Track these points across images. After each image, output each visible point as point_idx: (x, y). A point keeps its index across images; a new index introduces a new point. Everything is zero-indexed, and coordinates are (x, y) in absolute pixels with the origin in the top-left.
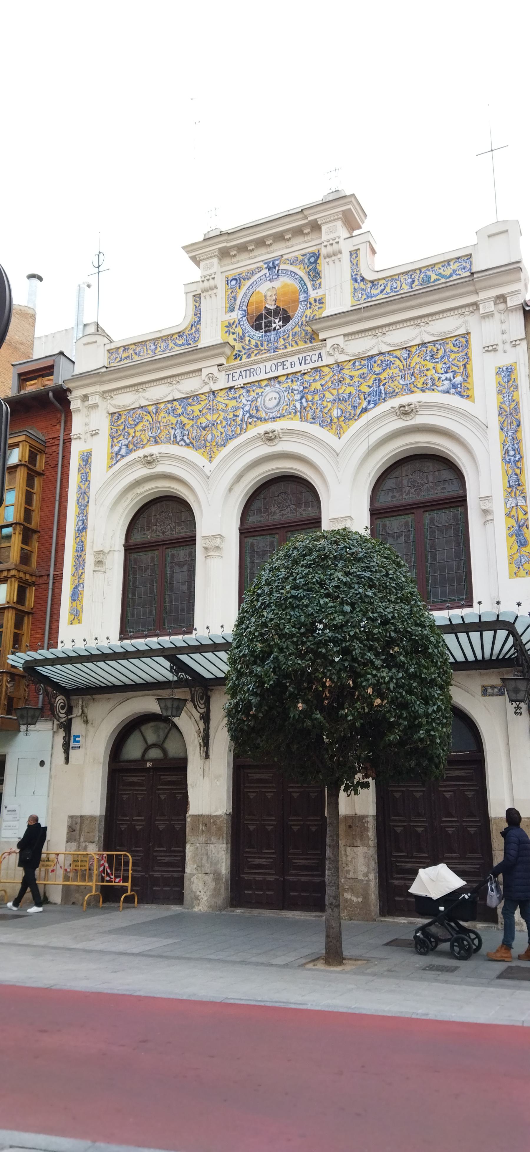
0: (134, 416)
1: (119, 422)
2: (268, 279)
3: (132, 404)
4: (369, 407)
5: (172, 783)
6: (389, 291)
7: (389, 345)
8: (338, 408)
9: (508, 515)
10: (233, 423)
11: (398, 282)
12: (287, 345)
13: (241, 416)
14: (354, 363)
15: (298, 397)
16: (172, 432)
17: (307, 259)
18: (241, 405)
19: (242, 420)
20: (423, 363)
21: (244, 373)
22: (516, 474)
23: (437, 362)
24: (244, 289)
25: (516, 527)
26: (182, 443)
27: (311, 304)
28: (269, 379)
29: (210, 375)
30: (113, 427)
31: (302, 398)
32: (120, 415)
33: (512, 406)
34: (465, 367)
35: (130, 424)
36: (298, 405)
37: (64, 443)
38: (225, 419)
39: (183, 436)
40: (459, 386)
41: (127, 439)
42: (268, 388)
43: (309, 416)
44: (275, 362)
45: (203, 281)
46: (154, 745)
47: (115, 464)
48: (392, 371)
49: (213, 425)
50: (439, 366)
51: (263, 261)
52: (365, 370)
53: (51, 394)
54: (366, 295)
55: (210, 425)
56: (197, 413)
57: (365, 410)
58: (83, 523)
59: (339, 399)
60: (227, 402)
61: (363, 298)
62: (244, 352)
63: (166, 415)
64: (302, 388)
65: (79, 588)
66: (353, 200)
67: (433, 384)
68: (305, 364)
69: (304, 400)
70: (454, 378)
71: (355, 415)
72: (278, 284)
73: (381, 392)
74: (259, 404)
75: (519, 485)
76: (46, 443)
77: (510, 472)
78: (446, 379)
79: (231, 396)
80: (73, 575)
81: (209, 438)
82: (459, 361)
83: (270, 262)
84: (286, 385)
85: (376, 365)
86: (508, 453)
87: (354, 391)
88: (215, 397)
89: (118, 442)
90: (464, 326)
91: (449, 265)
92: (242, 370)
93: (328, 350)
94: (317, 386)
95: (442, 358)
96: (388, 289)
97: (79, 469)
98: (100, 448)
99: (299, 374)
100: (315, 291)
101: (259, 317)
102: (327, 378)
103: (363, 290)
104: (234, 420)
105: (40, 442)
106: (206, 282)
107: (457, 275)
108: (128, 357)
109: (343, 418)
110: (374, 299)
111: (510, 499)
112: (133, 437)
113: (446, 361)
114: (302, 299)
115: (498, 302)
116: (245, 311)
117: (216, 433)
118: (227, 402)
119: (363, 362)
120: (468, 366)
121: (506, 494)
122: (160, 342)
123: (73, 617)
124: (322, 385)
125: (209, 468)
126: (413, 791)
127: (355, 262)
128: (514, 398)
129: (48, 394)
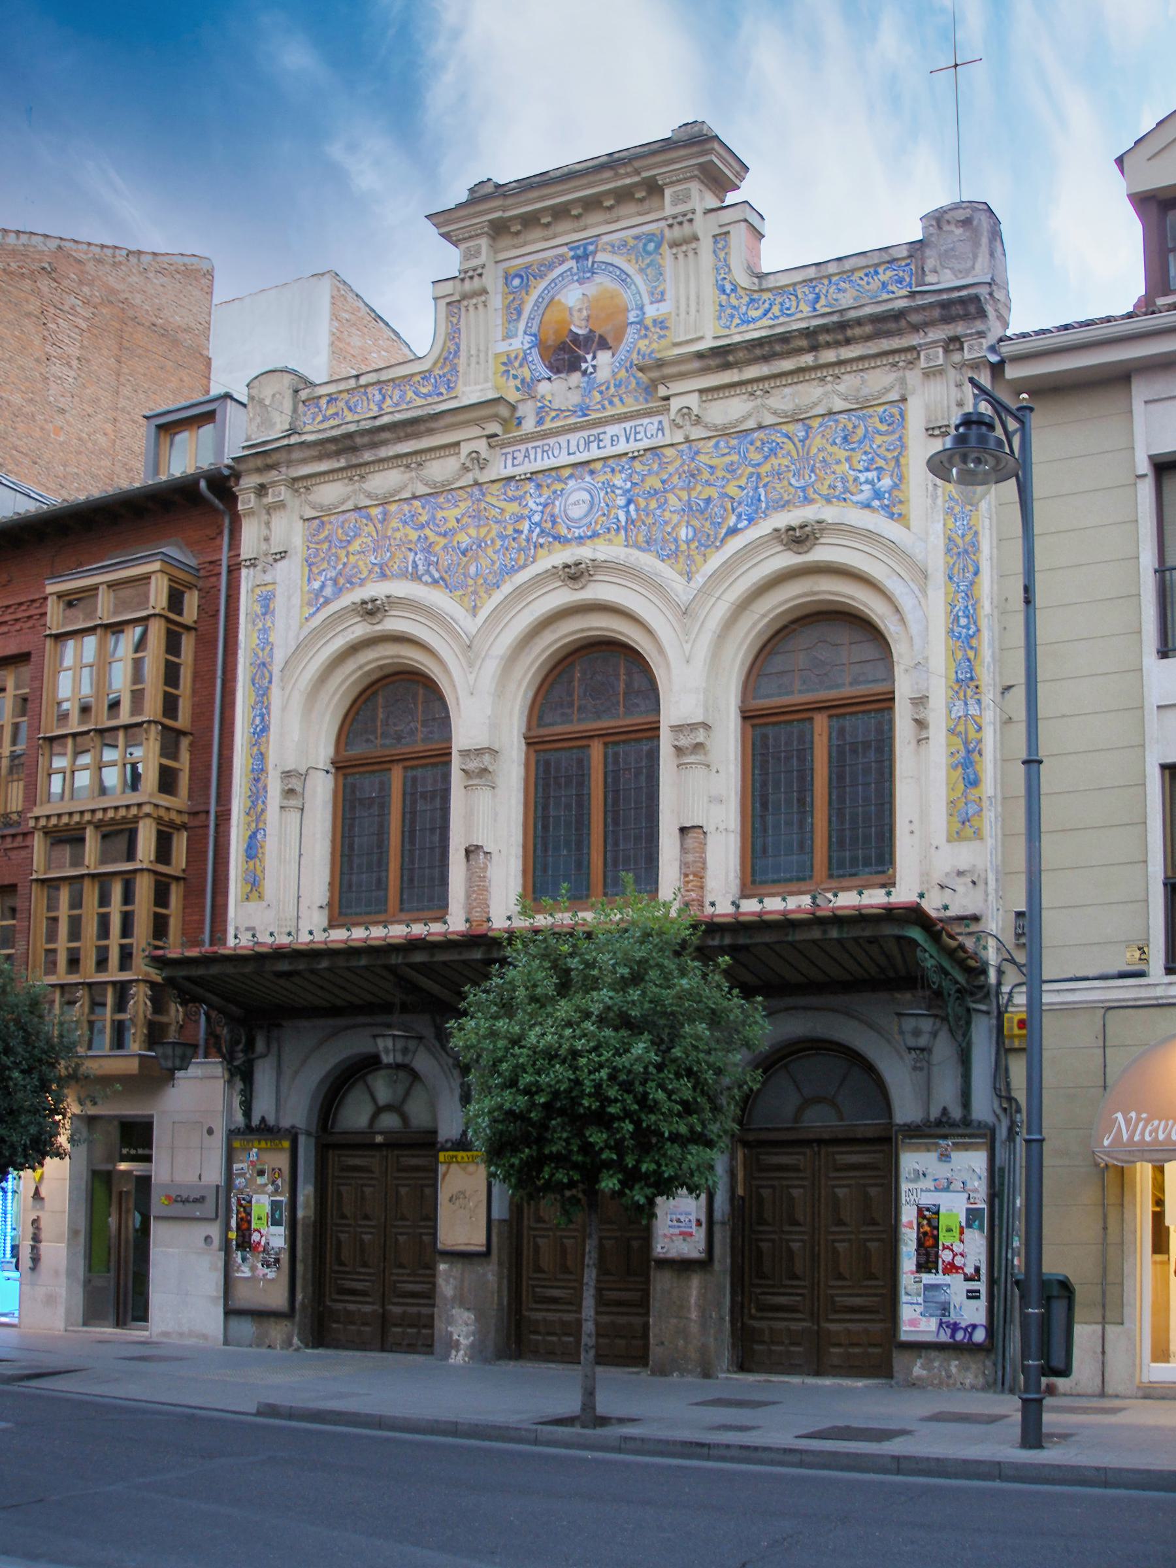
3: (342, 503)
5: (417, 1169)
6: (778, 314)
7: (775, 413)
8: (688, 524)
9: (952, 731)
10: (514, 545)
11: (793, 298)
12: (606, 402)
13: (526, 532)
14: (718, 443)
15: (621, 501)
16: (411, 556)
17: (641, 245)
18: (526, 512)
19: (528, 540)
20: (830, 449)
21: (532, 453)
22: (969, 660)
23: (853, 450)
24: (535, 294)
25: (963, 753)
26: (426, 578)
27: (647, 328)
28: (574, 465)
29: (474, 455)
30: (311, 545)
31: (629, 502)
32: (323, 523)
33: (968, 538)
35: (341, 541)
36: (622, 518)
37: (230, 572)
38: (502, 537)
39: (429, 565)
40: (887, 495)
41: (335, 568)
42: (572, 483)
43: (641, 539)
44: (585, 434)
45: (463, 280)
46: (389, 1108)
47: (314, 613)
48: (780, 461)
49: (480, 546)
51: (567, 244)
52: (735, 458)
53: (203, 484)
54: (740, 318)
55: (474, 547)
56: (452, 523)
57: (733, 531)
58: (262, 720)
59: (691, 508)
60: (503, 504)
61: (734, 324)
63: (400, 525)
65: (259, 837)
66: (716, 146)
67: (846, 490)
68: (636, 440)
69: (632, 507)
70: (879, 480)
71: (716, 538)
72: (591, 289)
73: (759, 500)
74: (557, 511)
75: (972, 679)
76: (198, 570)
77: (959, 655)
78: (867, 482)
79: (510, 494)
80: (248, 814)
81: (472, 570)
82: (888, 450)
83: (578, 248)
84: (602, 479)
85: (752, 448)
86: (958, 621)
87: (716, 495)
88: (484, 495)
89: (320, 573)
90: (897, 388)
91: (877, 273)
92: (530, 445)
93: (672, 417)
94: (654, 482)
95: (860, 442)
96: (776, 310)
98: (288, 577)
99: (624, 459)
100: (656, 306)
101: (562, 347)
102: (671, 469)
103: (734, 307)
104: (514, 539)
105: (187, 569)
106: (467, 281)
107: (888, 292)
108: (337, 414)
110: (752, 326)
111: (958, 703)
112: (345, 564)
113: (868, 449)
114: (632, 319)
115: (951, 347)
116: (535, 335)
117: (485, 562)
118: (503, 504)
119: (733, 442)
120: (902, 460)
121: (951, 693)
122: (390, 388)
124: (663, 482)
125: (469, 624)
126: (788, 1187)
128: (972, 523)
129: (197, 483)
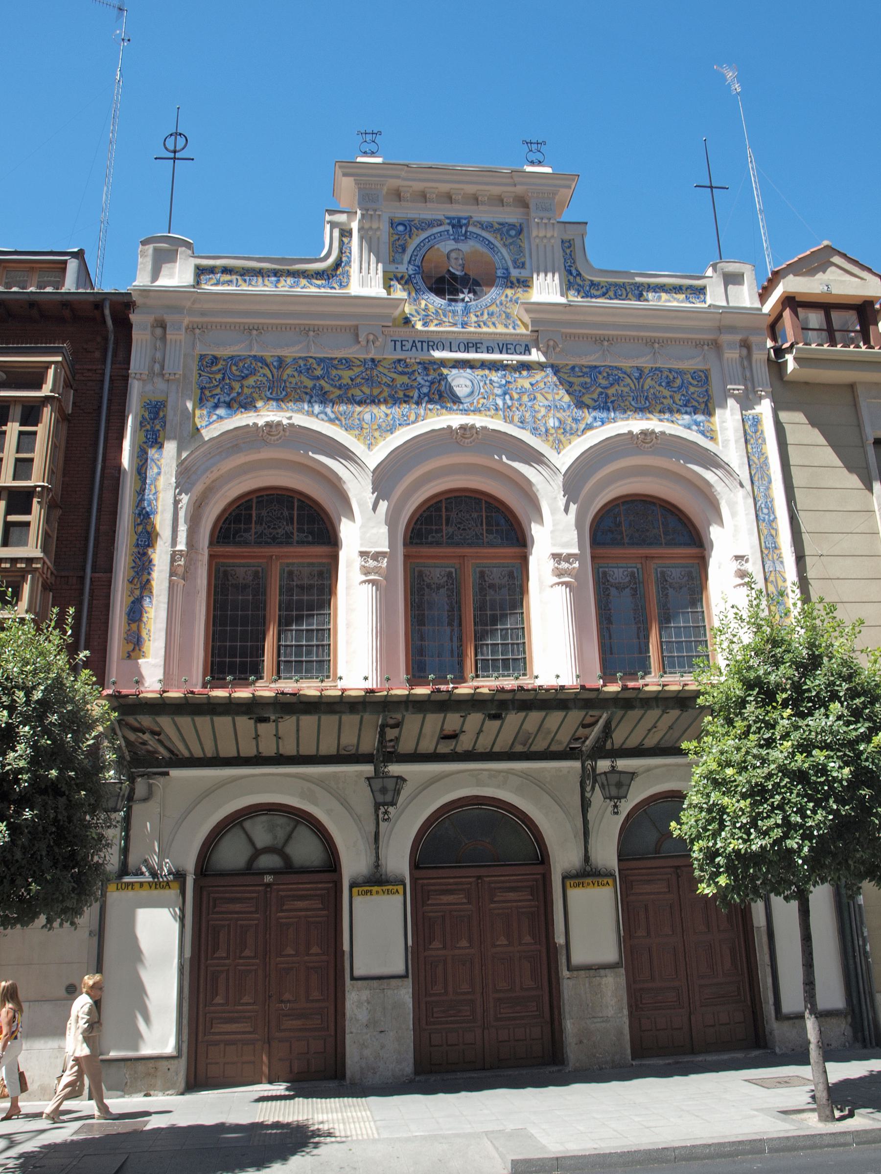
0: (241, 365)
1: (214, 369)
2: (452, 237)
4: (595, 424)
15: (499, 391)
22: (772, 536)
24: (416, 241)
26: (322, 416)
30: (203, 373)
31: (505, 394)
34: (706, 405)
41: (229, 395)
43: (516, 419)
50: (677, 397)
52: (588, 380)
57: (589, 427)
62: (419, 317)
63: (296, 374)
64: (504, 382)
69: (507, 397)
79: (400, 369)
83: (454, 218)
85: (601, 377)
88: (376, 366)
95: (680, 388)
97: (141, 423)
109: (562, 431)
112: (239, 394)
113: (684, 392)
116: (418, 267)
123: (131, 647)
124: (532, 385)
127: (568, 251)
